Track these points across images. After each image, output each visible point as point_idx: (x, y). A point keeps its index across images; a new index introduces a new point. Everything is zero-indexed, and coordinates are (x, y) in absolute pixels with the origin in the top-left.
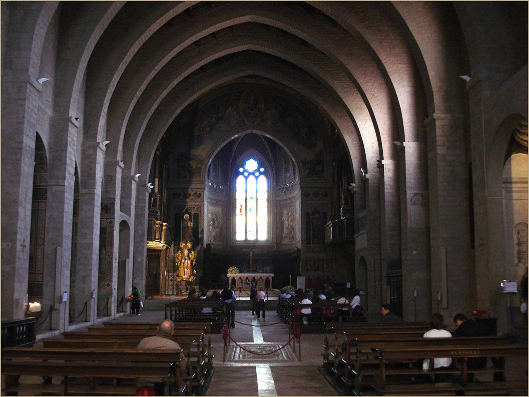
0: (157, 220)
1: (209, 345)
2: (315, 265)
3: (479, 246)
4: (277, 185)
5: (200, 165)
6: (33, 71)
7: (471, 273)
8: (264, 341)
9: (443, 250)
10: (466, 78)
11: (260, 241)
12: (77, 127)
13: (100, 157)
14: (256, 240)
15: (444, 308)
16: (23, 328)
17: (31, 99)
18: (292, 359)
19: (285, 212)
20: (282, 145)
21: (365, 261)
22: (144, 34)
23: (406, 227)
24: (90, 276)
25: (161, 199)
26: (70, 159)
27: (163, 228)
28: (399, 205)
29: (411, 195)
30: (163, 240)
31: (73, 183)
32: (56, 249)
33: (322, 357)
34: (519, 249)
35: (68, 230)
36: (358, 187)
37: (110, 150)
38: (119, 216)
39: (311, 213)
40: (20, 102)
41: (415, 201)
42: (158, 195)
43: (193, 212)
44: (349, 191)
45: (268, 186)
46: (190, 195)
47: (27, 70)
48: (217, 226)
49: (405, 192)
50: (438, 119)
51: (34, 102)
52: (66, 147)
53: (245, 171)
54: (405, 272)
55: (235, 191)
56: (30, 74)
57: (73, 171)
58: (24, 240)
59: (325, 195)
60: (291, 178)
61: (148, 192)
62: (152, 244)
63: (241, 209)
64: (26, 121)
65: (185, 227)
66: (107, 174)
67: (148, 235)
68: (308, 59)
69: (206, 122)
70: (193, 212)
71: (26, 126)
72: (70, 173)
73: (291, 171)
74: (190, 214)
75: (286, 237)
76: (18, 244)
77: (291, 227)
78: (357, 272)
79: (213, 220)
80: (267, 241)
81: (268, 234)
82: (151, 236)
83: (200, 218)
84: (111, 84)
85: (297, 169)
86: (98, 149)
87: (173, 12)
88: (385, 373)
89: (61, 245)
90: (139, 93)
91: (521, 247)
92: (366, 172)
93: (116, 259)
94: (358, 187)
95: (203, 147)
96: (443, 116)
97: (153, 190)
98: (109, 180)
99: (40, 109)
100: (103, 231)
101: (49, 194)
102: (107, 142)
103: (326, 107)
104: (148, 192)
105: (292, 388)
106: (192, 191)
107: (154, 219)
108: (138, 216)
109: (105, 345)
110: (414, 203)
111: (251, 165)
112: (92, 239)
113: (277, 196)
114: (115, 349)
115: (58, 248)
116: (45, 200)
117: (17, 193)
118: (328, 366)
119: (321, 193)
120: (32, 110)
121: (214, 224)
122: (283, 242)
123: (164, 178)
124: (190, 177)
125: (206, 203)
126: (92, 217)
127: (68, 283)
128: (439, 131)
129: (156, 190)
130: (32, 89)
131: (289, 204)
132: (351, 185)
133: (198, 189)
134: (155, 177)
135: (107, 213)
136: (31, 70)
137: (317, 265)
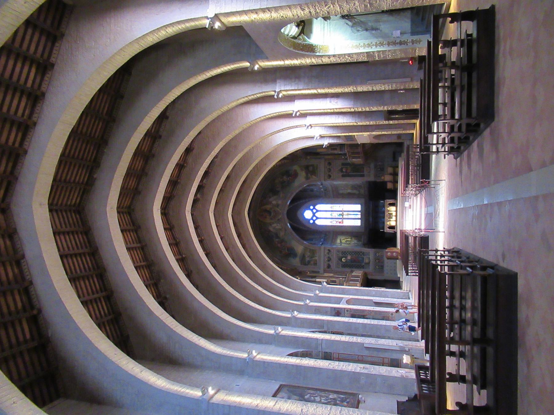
19: (341, 192)
32: (365, 347)
35: (354, 339)
39: (342, 174)
43: (341, 255)
53: (312, 219)
59: (330, 164)
70: (341, 255)
73: (313, 188)
75: (359, 191)
80: (361, 204)
90: (260, 288)
91: (369, 28)
93: (373, 308)
100: (353, 316)
108: (343, 292)
135: (341, 313)
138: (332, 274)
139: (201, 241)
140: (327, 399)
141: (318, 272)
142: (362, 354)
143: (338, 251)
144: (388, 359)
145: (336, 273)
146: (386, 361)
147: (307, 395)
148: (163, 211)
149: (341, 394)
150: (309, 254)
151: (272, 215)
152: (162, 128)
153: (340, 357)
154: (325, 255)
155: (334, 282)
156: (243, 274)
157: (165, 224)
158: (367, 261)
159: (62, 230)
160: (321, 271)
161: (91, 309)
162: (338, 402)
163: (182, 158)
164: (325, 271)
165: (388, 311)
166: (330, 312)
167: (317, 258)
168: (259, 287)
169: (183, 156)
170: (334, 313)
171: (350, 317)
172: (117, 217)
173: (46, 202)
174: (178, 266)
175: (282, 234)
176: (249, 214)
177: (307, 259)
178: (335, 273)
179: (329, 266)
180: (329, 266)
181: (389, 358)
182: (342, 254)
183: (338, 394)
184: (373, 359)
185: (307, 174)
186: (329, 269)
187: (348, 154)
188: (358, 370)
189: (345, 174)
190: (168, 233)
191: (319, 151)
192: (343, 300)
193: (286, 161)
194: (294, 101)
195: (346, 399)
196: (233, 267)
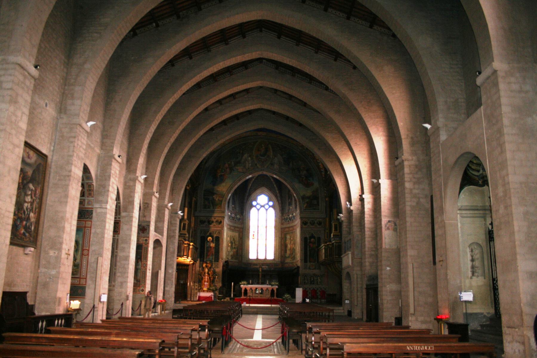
0: (186, 241)
2: (311, 279)
3: (440, 261)
5: (221, 199)
7: (434, 285)
10: (428, 126)
14: (266, 259)
15: (411, 314)
17: (80, 138)
19: (288, 237)
20: (286, 184)
21: (349, 274)
22: (177, 93)
23: (381, 247)
24: (126, 282)
26: (113, 188)
27: (190, 247)
29: (385, 222)
30: (190, 255)
31: (114, 207)
32: (98, 258)
34: (473, 264)
36: (345, 217)
37: (148, 182)
38: (153, 235)
39: (308, 238)
40: (72, 140)
41: (388, 227)
42: (187, 221)
43: (215, 236)
44: (338, 220)
45: (275, 216)
46: (213, 222)
48: (234, 248)
49: (381, 220)
51: (82, 140)
52: (110, 178)
53: (257, 204)
55: (249, 220)
58: (68, 250)
59: (320, 223)
60: (293, 210)
61: (179, 218)
62: (182, 260)
64: (75, 154)
65: (208, 247)
67: (178, 253)
69: (227, 165)
72: (112, 199)
73: (293, 205)
74: (212, 237)
75: (289, 257)
76: (64, 252)
77: (293, 249)
79: (231, 243)
80: (274, 259)
81: (275, 254)
83: (221, 240)
85: (298, 204)
86: (137, 182)
87: (199, 77)
89: (102, 256)
91: (474, 263)
92: (351, 205)
93: (149, 270)
94: (345, 217)
95: (224, 184)
96: (410, 158)
97: (183, 216)
98: (145, 207)
101: (94, 214)
103: (319, 154)
104: (179, 218)
106: (215, 219)
107: (183, 240)
108: (170, 237)
110: (388, 229)
111: (262, 199)
112: (129, 252)
113: (282, 224)
115: (100, 258)
116: (91, 219)
117: (65, 212)
119: (316, 222)
120: (81, 147)
121: (232, 246)
122: (286, 261)
124: (213, 208)
125: (225, 228)
126: (130, 236)
128: (406, 170)
129: (186, 217)
130: (82, 130)
132: (339, 216)
133: (219, 217)
134: (185, 207)
135: (143, 233)
137: (312, 280)
138: (193, 226)
140: (29, 210)
141: (195, 210)
142: (90, 254)
143: (219, 232)
144: (84, 283)
147: (33, 186)
149: (35, 227)
151: (261, 157)
153: (86, 228)
162: (24, 223)
164: (196, 217)
166: (145, 220)
170: (144, 224)
171: (137, 244)
175: (240, 168)
181: (85, 285)
183: (36, 223)
185: (308, 198)
187: (330, 244)
189: (308, 241)
191: (335, 211)
192: (160, 236)
194: (388, 179)
195: (29, 233)
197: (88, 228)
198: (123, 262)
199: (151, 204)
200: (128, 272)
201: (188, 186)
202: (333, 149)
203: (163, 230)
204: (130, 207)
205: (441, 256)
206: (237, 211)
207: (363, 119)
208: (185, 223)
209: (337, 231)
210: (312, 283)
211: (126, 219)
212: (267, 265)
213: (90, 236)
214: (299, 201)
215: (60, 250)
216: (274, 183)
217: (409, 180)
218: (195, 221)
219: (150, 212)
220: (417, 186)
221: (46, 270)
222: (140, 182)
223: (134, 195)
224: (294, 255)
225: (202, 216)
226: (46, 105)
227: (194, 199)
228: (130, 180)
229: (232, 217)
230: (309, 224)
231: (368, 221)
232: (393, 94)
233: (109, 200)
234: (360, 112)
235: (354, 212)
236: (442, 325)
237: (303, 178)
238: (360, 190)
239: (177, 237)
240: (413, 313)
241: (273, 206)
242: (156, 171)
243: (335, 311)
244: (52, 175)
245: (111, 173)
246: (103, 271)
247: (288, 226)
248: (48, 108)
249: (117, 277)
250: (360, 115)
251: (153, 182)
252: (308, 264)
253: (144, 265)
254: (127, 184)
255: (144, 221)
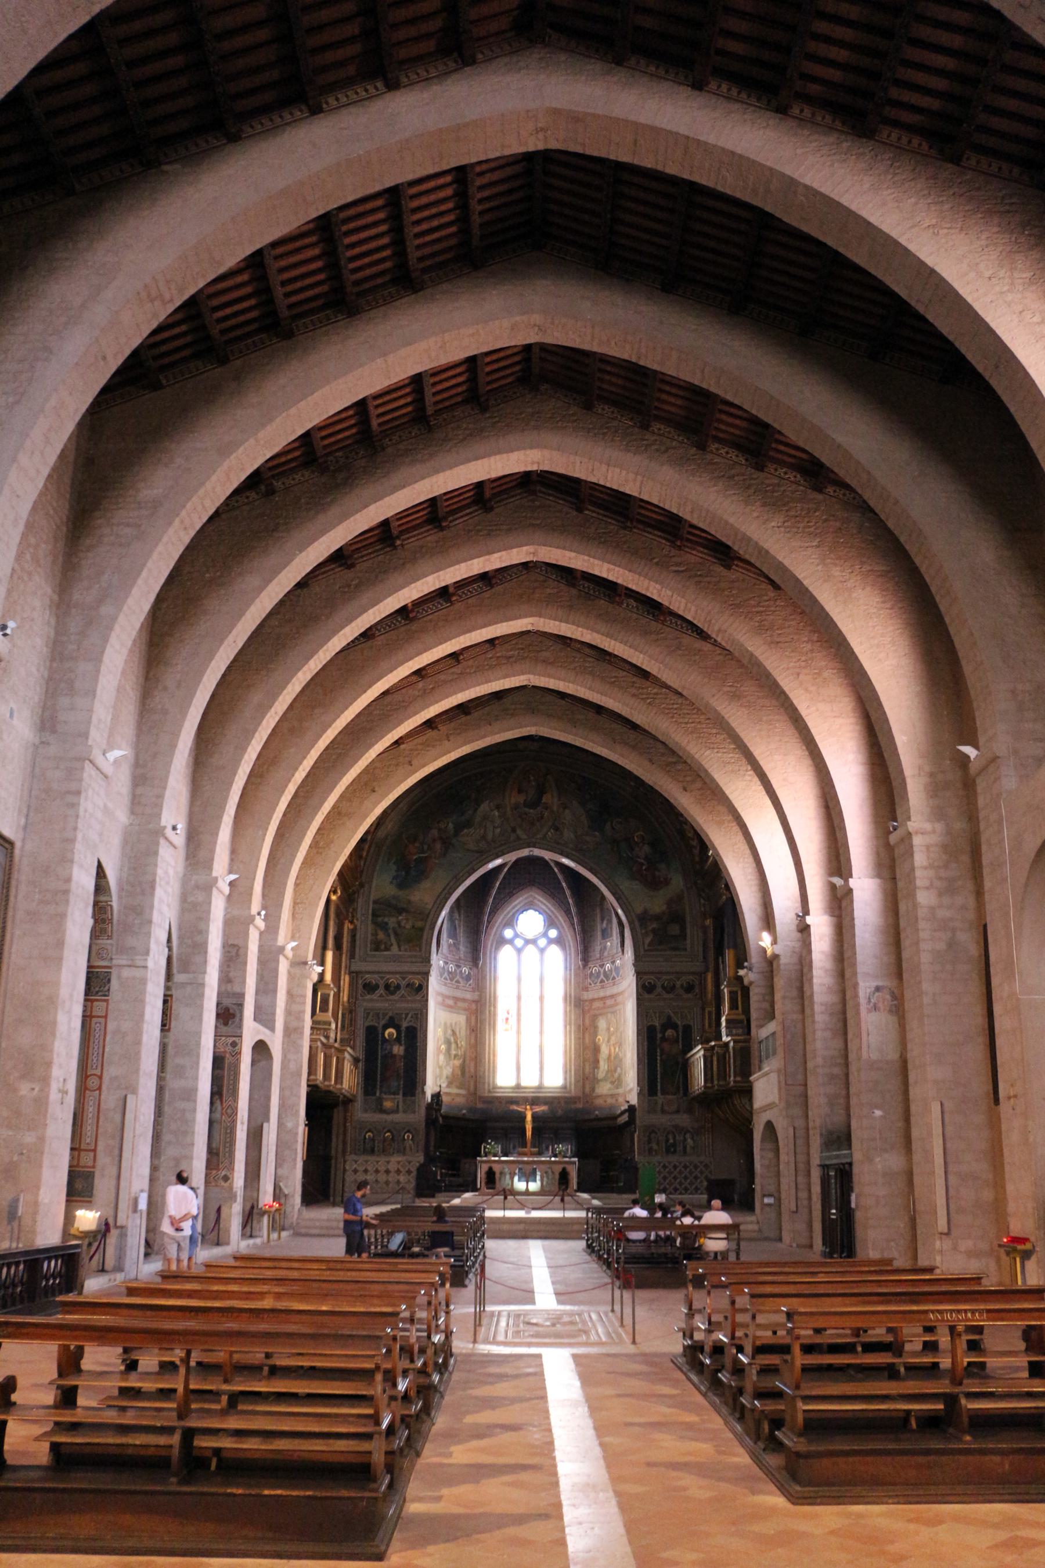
1: (447, 1306)
2: (667, 1141)
3: (1009, 1098)
4: (585, 965)
5: (419, 924)
6: (97, 736)
8: (539, 1356)
9: (936, 1108)
11: (501, 1088)
12: (175, 847)
13: (218, 908)
16: (56, 1264)
17: (90, 792)
18: (617, 1341)
19: (602, 1024)
23: (859, 1059)
25: (337, 996)
26: (161, 913)
28: (844, 1012)
29: (868, 991)
33: (681, 1334)
35: (149, 1062)
38: (251, 1031)
40: (70, 799)
43: (405, 1025)
44: (740, 979)
47: (86, 735)
48: (456, 1056)
49: (856, 986)
50: (916, 833)
53: (516, 935)
54: (857, 1156)
56: (90, 742)
57: (164, 937)
58: (65, 1080)
59: (689, 988)
63: (507, 1019)
64: (80, 836)
66: (230, 942)
68: (649, 704)
70: (405, 1025)
71: (78, 846)
74: (397, 1028)
75: (605, 1079)
76: (54, 1087)
78: (757, 1157)
79: (448, 1043)
80: (564, 1087)
82: (316, 1074)
84: (246, 757)
86: (215, 891)
88: (799, 1359)
89: (135, 1092)
90: (300, 776)
95: (426, 884)
96: (928, 826)
97: (322, 975)
98: (233, 955)
99: (106, 810)
100: (218, 1062)
101: (114, 984)
102: (233, 877)
103: (686, 802)
105: (619, 1396)
108: (291, 1032)
109: (248, 1296)
110: (875, 1008)
114: (267, 1303)
115: (129, 1097)
117: (57, 984)
118: (694, 1350)
121: (448, 1050)
123: (345, 951)
126: (198, 1034)
127: (146, 1171)
128: (920, 858)
129: (328, 977)
130: (94, 772)
131: (609, 1004)
135: (226, 1024)
136: (94, 733)
138: (346, 999)
139: (443, 593)
142: (104, 1087)
144: (91, 1164)
145: (351, 1012)
146: (86, 1159)
148: (534, 478)
150: (408, 927)
152: (786, 473)
153: (94, 1020)
154: (403, 974)
155: (320, 1004)
156: (344, 724)
157: (495, 484)
158: (388, 1104)
159: (472, 190)
160: (358, 966)
161: (239, 279)
163: (697, 532)
164: (354, 975)
165: (236, 1168)
167: (395, 949)
168: (304, 774)
169: (703, 535)
170: (227, 1002)
171: (214, 1053)
172: (513, 344)
173: (553, 145)
174: (366, 528)
176: (529, 738)
177: (392, 922)
178: (351, 1011)
179: (370, 988)
180: (370, 988)
181: (94, 1167)
182: (407, 1028)
184: (90, 1121)
185: (657, 918)
186: (360, 987)
188: (56, 1072)
189: (659, 1036)
190: (466, 496)
191: (729, 956)
192: (267, 1032)
193: (696, 851)
196: (365, 692)
197: (100, 1020)
198: (181, 1105)
199: (247, 948)
200: (193, 1133)
201: (335, 892)
202: (724, 793)
203: (274, 1014)
204: (198, 959)
205: (1012, 1085)
206: (462, 956)
207: (803, 720)
208: (327, 992)
209: (737, 1008)
210: (671, 1149)
211: (189, 989)
212: (545, 1103)
213: (104, 1040)
214: (632, 930)
215: (45, 1080)
216: (560, 876)
217: (927, 883)
218: (351, 984)
219: (245, 971)
220: (946, 900)
221: (11, 1133)
222: (221, 892)
223: (208, 926)
224: (620, 1075)
225: (369, 973)
226: (11, 716)
227: (347, 926)
228: (197, 887)
229: (450, 973)
230: (659, 990)
231: (821, 985)
232: (880, 660)
233: (153, 946)
234: (795, 702)
235: (783, 960)
236: (1018, 1260)
237: (642, 864)
238: (799, 899)
239: (307, 1031)
240: (946, 1231)
241: (559, 941)
242: (258, 860)
243: (742, 1227)
244: (23, 889)
245: (155, 874)
246: (137, 1132)
247: (602, 994)
248: (15, 722)
249: (163, 1144)
250: (796, 709)
251: (252, 888)
252: (660, 1098)
253: (229, 1111)
254: (190, 899)
255: (228, 993)
